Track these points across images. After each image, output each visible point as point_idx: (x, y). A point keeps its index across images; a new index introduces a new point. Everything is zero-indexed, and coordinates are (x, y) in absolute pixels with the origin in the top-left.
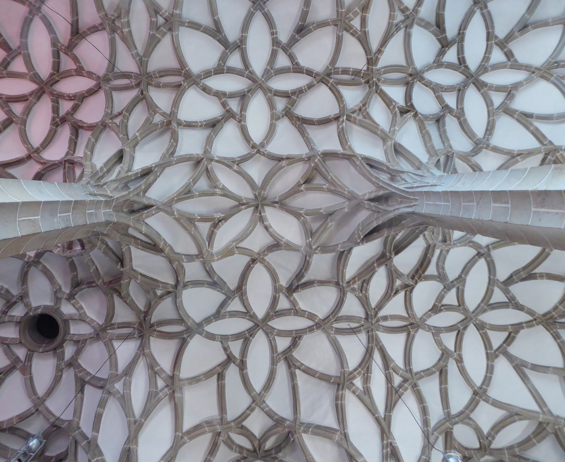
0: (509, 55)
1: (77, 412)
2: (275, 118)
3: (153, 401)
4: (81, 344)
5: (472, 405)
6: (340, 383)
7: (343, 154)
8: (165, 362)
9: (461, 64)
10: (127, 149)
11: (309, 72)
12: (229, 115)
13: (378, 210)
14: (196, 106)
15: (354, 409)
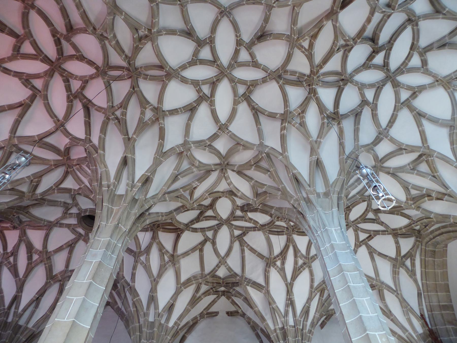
0: (424, 63)
3: (163, 269)
6: (285, 118)
8: (169, 246)
9: (384, 66)
10: (129, 155)
11: (265, 69)
12: (202, 98)
14: (178, 95)
15: (274, 275)
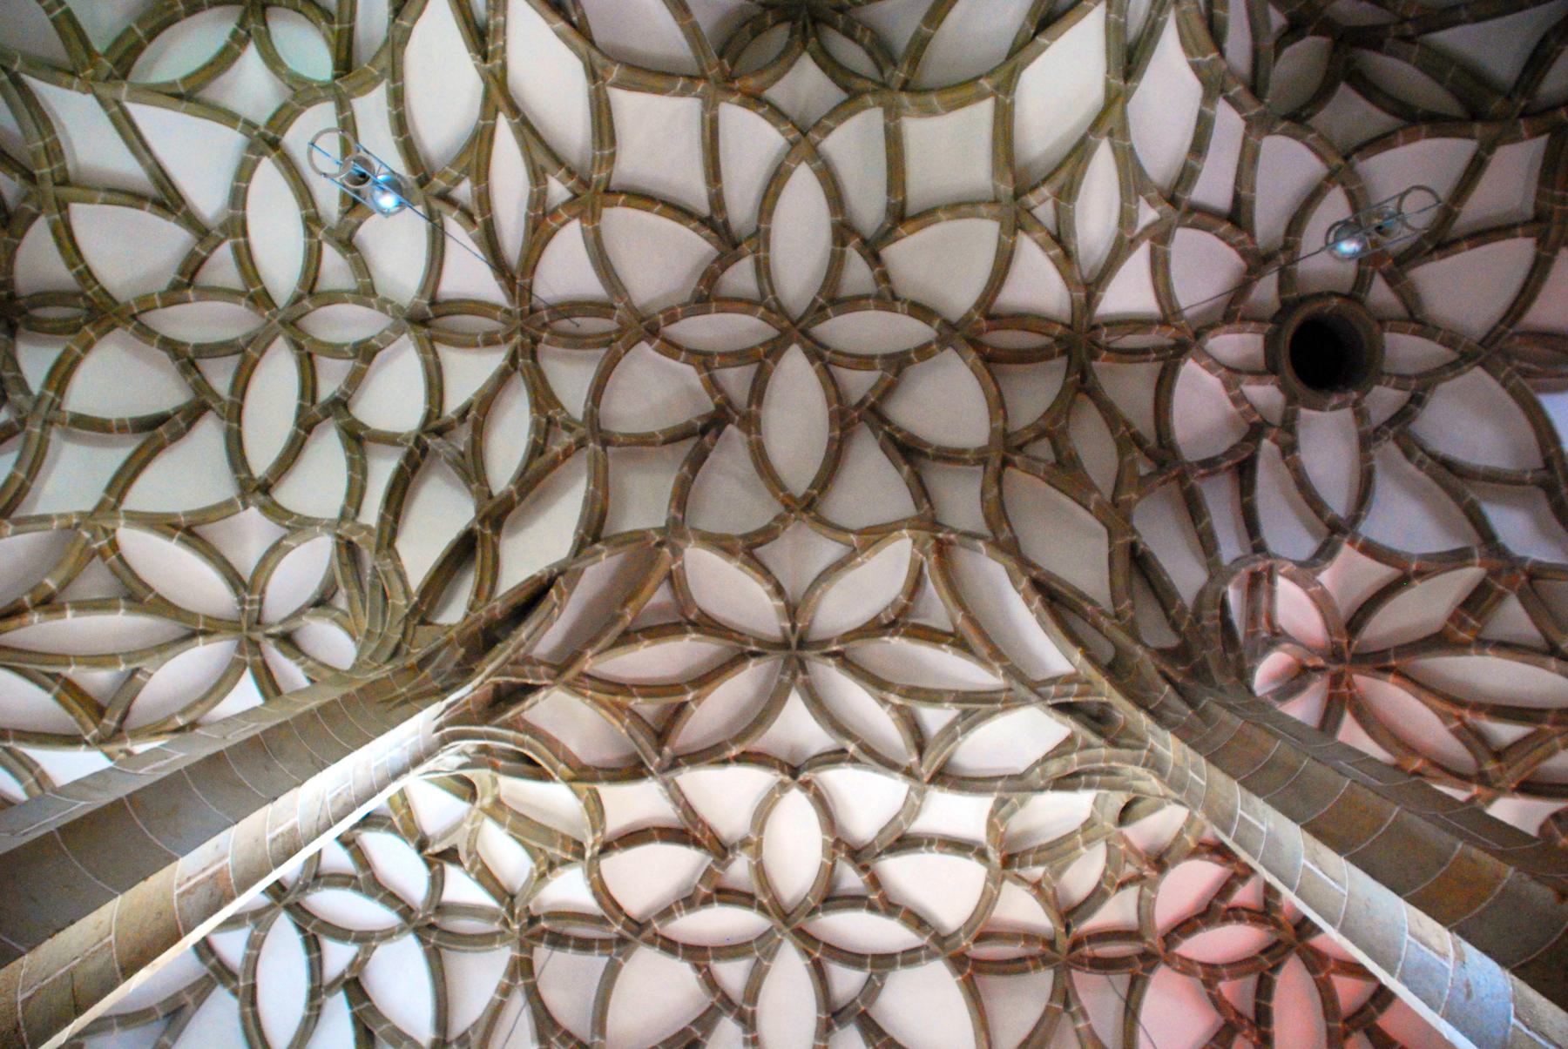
1: (1248, 160)
2: (752, 844)
4: (1232, 310)
5: (284, 117)
7: (595, 780)
11: (670, 946)
13: (517, 668)
